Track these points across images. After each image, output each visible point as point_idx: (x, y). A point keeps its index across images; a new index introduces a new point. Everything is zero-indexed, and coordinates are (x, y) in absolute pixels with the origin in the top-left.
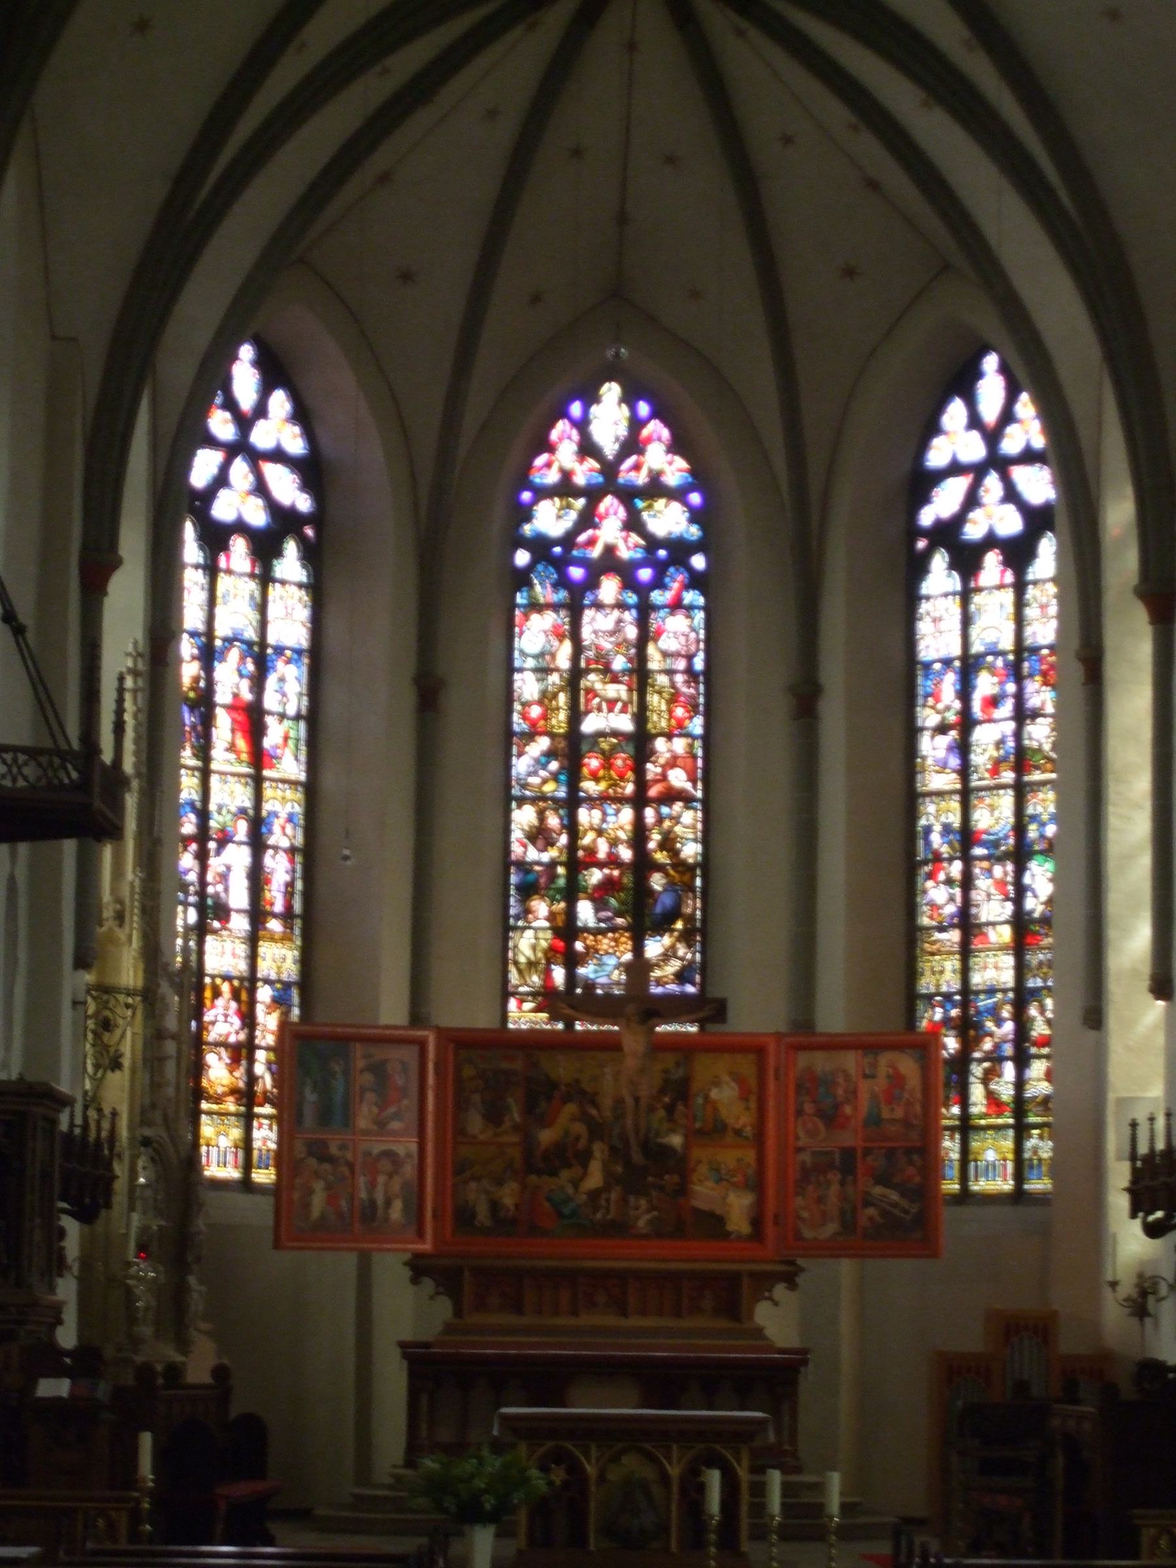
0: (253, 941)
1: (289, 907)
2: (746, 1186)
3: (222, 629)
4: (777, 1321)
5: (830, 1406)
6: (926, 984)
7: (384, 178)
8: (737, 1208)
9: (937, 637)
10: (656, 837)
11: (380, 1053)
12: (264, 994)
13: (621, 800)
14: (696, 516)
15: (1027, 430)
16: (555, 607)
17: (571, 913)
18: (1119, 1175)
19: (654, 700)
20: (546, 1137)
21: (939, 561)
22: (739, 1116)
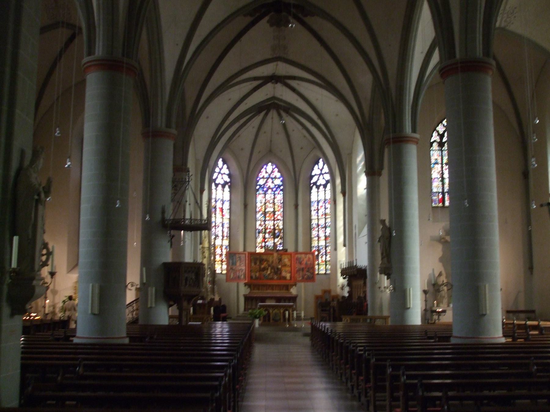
0: (222, 239)
2: (289, 273)
4: (294, 291)
5: (301, 302)
6: (313, 245)
7: (239, 136)
8: (288, 276)
9: (314, 197)
11: (240, 255)
12: (224, 247)
14: (281, 181)
15: (326, 169)
18: (339, 271)
20: (262, 266)
21: (314, 187)
22: (288, 263)
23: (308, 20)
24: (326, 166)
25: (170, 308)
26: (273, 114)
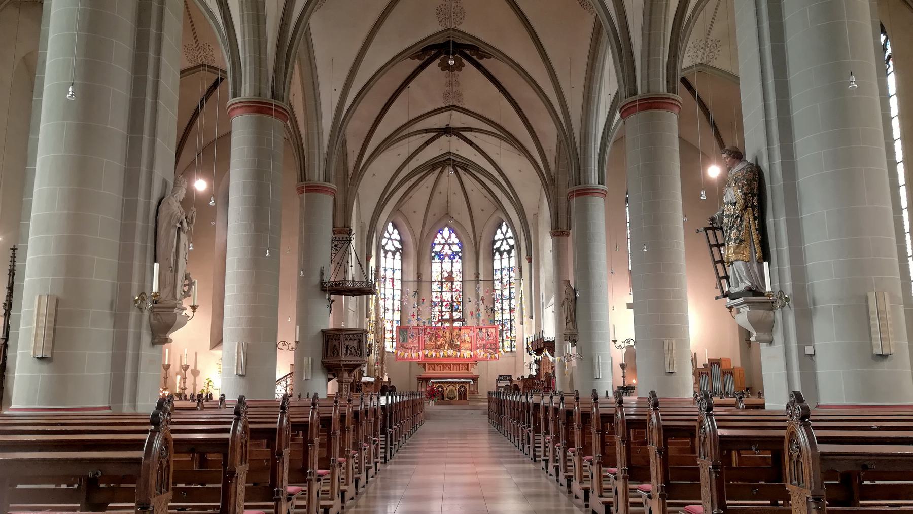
9: (497, 265)
23: (483, 62)
24: (509, 230)
25: (330, 383)
26: (450, 172)
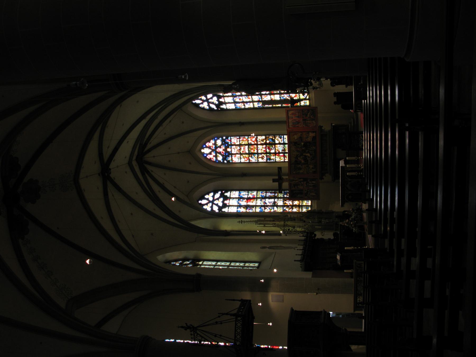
1: (274, 193)
3: (237, 204)
8: (311, 135)
9: (232, 106)
10: (262, 142)
13: (257, 147)
16: (232, 157)
17: (273, 153)
19: (243, 143)
20: (303, 162)
